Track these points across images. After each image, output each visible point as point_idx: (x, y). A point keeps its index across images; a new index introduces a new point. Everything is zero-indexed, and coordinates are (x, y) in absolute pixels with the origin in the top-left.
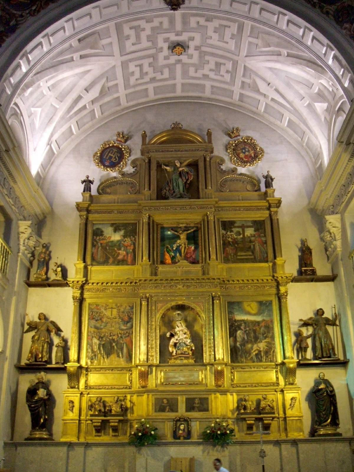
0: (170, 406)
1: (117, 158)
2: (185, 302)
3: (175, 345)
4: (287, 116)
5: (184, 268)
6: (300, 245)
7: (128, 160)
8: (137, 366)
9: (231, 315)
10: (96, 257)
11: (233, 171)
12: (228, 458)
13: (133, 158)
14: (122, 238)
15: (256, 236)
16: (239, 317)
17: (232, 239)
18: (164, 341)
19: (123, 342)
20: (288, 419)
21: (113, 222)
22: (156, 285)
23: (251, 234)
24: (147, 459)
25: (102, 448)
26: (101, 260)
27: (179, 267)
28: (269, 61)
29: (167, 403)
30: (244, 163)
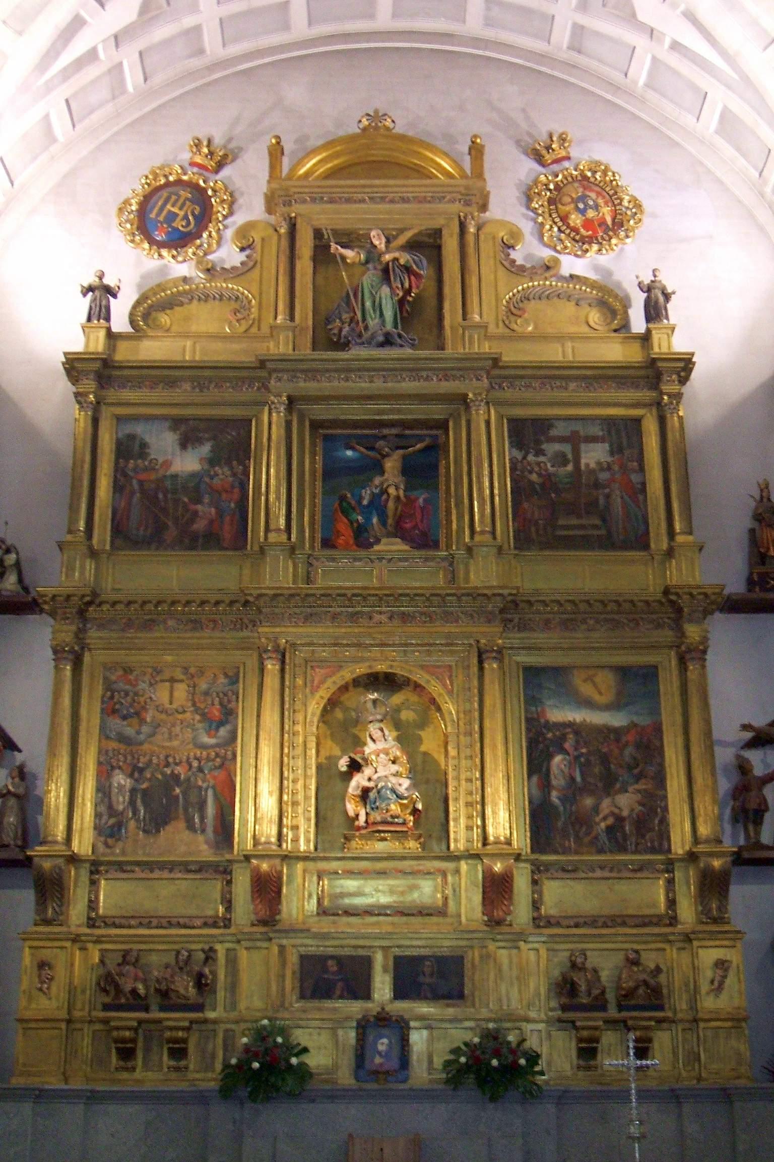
3: (365, 794)
4: (719, 98)
7: (226, 227)
11: (548, 268)
13: (239, 219)
14: (206, 467)
19: (205, 785)
23: (599, 463)
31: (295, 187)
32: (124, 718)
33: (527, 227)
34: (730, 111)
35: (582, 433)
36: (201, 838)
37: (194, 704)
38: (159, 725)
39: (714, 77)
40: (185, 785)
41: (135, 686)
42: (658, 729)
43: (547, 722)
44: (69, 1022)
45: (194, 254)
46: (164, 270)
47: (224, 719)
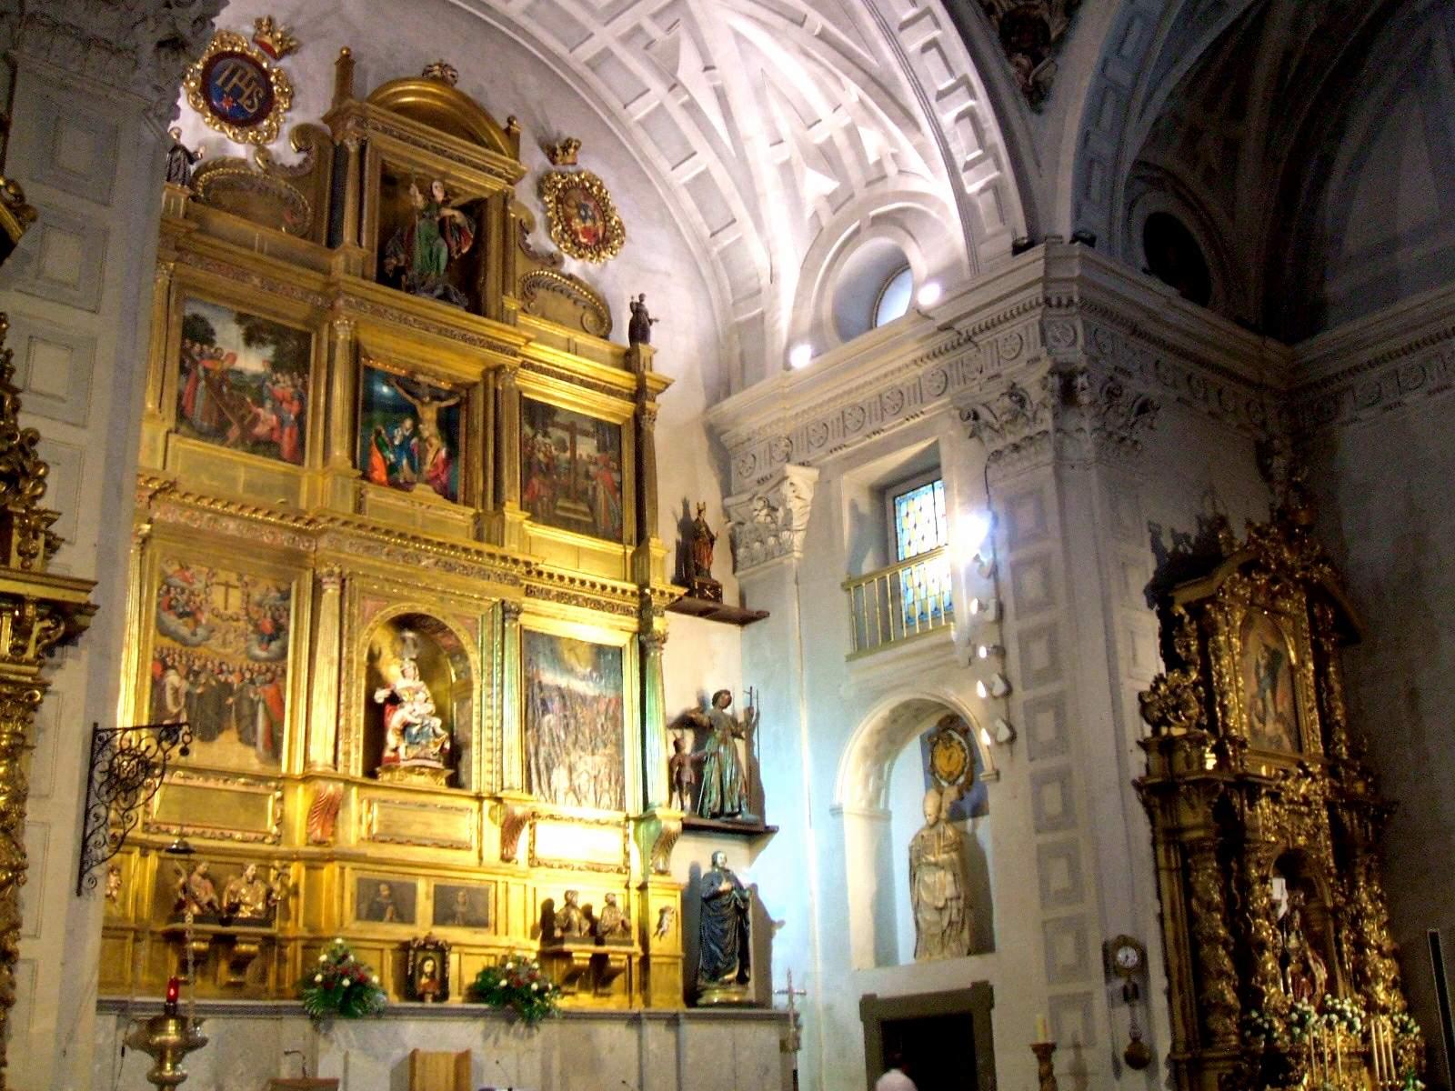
0: (394, 904)
3: (406, 727)
4: (705, 159)
6: (680, 516)
10: (189, 408)
12: (538, 1056)
13: (297, 118)
14: (269, 370)
15: (601, 464)
16: (550, 677)
18: (376, 717)
19: (256, 698)
20: (653, 960)
21: (244, 311)
22: (368, 543)
23: (589, 456)
24: (346, 1056)
28: (750, 17)
30: (579, 249)
32: (181, 616)
33: (539, 217)
35: (578, 426)
36: (251, 752)
37: (248, 614)
39: (710, 141)
41: (191, 584)
46: (221, 144)
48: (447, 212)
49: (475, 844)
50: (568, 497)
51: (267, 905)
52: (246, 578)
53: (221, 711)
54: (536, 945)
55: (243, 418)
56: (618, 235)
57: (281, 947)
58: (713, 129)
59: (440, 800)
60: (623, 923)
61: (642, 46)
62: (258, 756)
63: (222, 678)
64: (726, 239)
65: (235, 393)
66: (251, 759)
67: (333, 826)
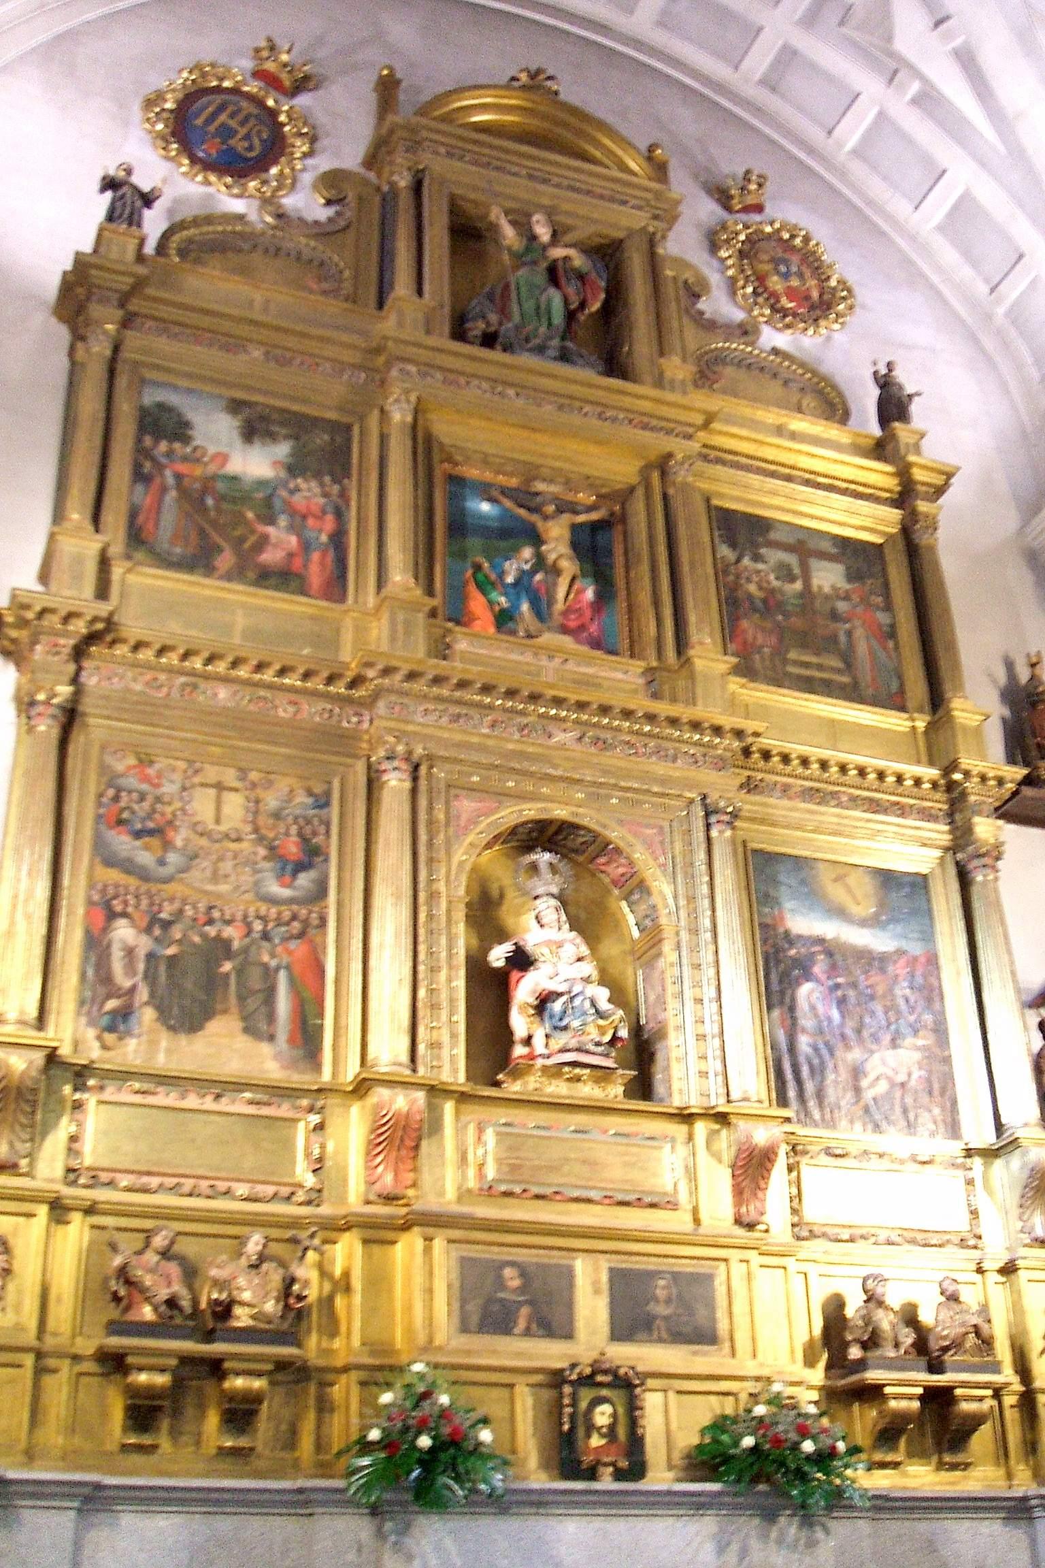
1: (256, 142)
2: (581, 810)
3: (542, 1003)
4: (962, 175)
5: (570, 666)
6: (1002, 677)
7: (304, 170)
8: (361, 1088)
9: (767, 910)
10: (150, 526)
11: (746, 333)
13: (323, 163)
14: (283, 474)
15: (856, 598)
16: (803, 922)
17: (760, 588)
18: (490, 989)
19: (273, 963)
21: (240, 395)
22: (457, 710)
23: (833, 587)
25: (177, 1519)
26: (178, 550)
27: (551, 658)
29: (522, 1289)
31: (431, 130)
32: (138, 835)
34: (974, 199)
36: (265, 1048)
37: (256, 830)
38: (196, 856)
40: (241, 957)
41: (158, 786)
42: (933, 960)
43: (787, 933)
44: (39, 1355)
45: (259, 190)
47: (306, 860)
48: (558, 253)
49: (683, 1198)
50: (804, 645)
51: (287, 1307)
52: (254, 776)
53: (213, 984)
54: (817, 1375)
55: (242, 540)
56: (844, 298)
57: (324, 1385)
58: (964, 121)
59: (614, 1123)
60: (977, 1330)
61: (835, 20)
62: (277, 1056)
63: (211, 931)
64: (1013, 290)
65: (225, 506)
66: (268, 1062)
67: (415, 1169)
